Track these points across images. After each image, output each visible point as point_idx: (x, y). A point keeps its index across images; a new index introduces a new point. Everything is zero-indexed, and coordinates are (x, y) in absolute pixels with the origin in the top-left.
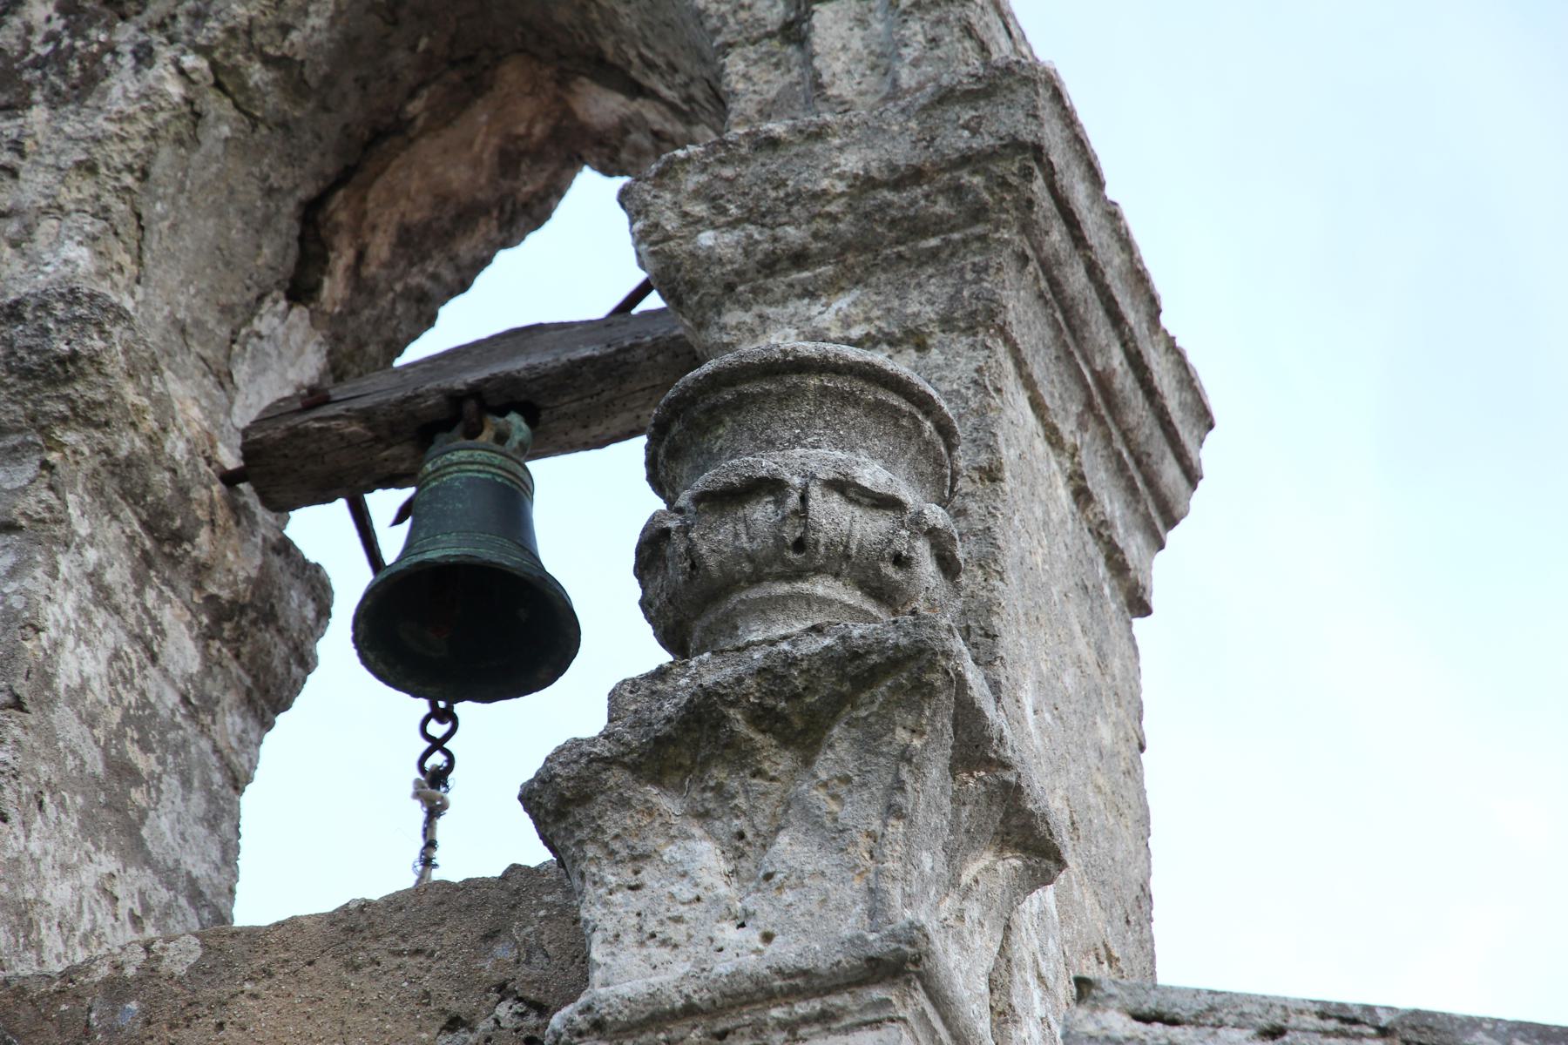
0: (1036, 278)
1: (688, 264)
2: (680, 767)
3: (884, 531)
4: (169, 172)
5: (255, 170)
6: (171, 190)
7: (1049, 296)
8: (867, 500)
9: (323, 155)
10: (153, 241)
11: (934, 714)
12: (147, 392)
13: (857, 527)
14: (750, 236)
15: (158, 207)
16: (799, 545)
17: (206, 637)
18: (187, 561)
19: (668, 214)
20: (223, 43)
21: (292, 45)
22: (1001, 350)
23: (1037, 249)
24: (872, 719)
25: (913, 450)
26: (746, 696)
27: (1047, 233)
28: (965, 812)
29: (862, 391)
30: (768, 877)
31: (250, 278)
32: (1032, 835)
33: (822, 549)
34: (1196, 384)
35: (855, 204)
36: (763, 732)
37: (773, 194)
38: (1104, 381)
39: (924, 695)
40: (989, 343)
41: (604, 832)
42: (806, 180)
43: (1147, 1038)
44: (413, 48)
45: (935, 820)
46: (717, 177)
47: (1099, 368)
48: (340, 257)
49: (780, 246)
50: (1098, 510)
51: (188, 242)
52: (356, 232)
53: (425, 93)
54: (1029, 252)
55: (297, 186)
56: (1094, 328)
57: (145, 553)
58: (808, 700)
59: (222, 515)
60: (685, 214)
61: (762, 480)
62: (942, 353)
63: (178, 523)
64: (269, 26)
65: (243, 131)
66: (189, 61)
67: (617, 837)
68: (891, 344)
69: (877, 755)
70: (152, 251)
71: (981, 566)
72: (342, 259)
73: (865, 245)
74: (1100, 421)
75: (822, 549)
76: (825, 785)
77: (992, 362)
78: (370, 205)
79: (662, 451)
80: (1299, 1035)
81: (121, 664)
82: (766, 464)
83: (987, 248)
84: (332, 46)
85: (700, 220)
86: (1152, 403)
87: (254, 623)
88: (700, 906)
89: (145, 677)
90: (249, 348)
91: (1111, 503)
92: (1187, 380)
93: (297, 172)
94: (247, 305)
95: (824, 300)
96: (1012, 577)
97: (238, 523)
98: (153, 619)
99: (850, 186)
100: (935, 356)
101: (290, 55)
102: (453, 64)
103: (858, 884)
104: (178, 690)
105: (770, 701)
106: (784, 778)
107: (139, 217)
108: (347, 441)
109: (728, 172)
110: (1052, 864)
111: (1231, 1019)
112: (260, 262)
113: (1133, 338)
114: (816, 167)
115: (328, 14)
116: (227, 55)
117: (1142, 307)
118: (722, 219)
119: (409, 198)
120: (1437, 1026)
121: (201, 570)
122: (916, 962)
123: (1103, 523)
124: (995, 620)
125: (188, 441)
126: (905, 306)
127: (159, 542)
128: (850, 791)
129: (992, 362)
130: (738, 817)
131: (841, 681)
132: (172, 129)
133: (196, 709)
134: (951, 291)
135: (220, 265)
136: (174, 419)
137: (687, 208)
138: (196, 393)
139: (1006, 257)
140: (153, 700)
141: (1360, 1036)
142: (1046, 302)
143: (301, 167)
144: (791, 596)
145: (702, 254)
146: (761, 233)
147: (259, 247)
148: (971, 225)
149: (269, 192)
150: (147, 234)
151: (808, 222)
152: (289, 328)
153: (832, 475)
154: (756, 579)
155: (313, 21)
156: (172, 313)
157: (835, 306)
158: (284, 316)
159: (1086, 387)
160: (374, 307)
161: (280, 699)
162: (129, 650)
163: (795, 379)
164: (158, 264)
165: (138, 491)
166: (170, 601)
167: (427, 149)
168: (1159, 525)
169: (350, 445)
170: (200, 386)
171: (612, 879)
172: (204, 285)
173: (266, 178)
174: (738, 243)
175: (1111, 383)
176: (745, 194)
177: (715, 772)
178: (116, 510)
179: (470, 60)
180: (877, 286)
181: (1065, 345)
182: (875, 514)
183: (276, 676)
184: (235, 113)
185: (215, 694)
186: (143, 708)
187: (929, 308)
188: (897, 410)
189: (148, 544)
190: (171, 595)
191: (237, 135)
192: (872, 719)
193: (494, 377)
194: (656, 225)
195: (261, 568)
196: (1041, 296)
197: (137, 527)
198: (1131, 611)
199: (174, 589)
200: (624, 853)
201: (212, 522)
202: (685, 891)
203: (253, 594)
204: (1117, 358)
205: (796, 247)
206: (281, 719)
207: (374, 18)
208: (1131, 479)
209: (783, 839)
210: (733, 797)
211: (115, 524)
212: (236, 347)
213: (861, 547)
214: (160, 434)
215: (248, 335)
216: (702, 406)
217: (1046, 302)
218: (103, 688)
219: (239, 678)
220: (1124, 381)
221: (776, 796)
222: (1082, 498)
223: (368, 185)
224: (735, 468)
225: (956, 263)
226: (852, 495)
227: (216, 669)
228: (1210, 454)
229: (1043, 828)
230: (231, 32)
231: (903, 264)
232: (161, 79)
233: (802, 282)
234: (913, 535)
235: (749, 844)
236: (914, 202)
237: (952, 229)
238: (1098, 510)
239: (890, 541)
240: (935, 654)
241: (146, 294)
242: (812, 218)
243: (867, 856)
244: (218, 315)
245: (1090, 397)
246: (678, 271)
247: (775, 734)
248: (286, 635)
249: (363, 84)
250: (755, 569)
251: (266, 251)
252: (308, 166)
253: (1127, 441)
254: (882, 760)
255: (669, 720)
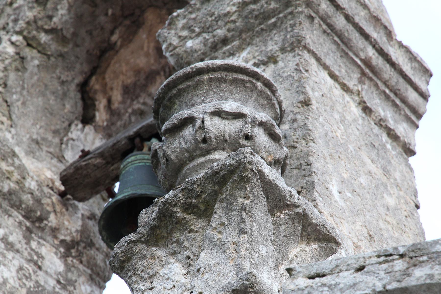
0: (320, 25)
1: (185, 56)
2: (163, 237)
3: (238, 127)
4: (15, 82)
5: (54, 75)
6: (19, 89)
7: (329, 31)
8: (230, 117)
9: (81, 64)
10: (16, 111)
11: (252, 188)
12: (13, 165)
13: (227, 128)
14: (205, 38)
15: (15, 97)
16: (204, 141)
17: (65, 257)
18: (47, 228)
19: (174, 38)
20: (26, 28)
21: (55, 23)
22: (306, 55)
23: (317, 13)
24: (228, 197)
25: (255, 95)
26: (179, 201)
27: (319, 5)
28: (282, 228)
29: (226, 76)
30: (199, 270)
31: (63, 117)
32: (320, 234)
33: (214, 140)
34: (419, 59)
35: (241, 14)
36: (190, 214)
37: (210, 19)
38: (367, 62)
39: (245, 182)
40: (300, 53)
41: (138, 270)
42: (222, 10)
43: (313, 285)
44: (106, 14)
45: (264, 232)
46: (190, 19)
47: (363, 58)
48: (100, 102)
49: (216, 38)
50: (377, 115)
51: (31, 108)
52: (105, 92)
53: (117, 31)
54: (313, 14)
55: (74, 79)
56: (355, 41)
57: (28, 228)
58: (204, 196)
59: (58, 208)
60: (180, 37)
61: (186, 119)
62: (283, 62)
63: (39, 213)
64: (43, 18)
65: (44, 61)
66: (14, 38)
67: (143, 271)
68: (264, 64)
69: (233, 211)
70: (16, 114)
71: (304, 139)
72: (101, 104)
73: (248, 29)
74: (371, 79)
75: (214, 140)
76: (215, 228)
77: (302, 60)
78: (107, 80)
79: (159, 122)
80: (370, 266)
81: (23, 272)
82: (186, 113)
83: (294, 16)
84: (72, 20)
85: (185, 38)
86: (395, 69)
87: (85, 248)
88: (175, 289)
89: (37, 276)
90: (69, 145)
91: (384, 111)
92: (413, 58)
93: (72, 73)
94: (65, 129)
95: (237, 55)
96: (320, 141)
97: (67, 210)
98: (37, 254)
99: (238, 7)
100: (281, 64)
101: (55, 27)
102: (126, 17)
103: (232, 263)
104: (55, 279)
105: (189, 201)
106: (201, 230)
107: (6, 102)
108: (97, 167)
109: (193, 16)
110: (333, 245)
111: (344, 268)
112: (66, 111)
113: (377, 43)
114: (224, 4)
115: (66, 8)
116: (29, 33)
117: (381, 31)
118: (194, 35)
119: (123, 74)
120: (422, 248)
121: (54, 231)
122: (252, 287)
123: (381, 120)
124: (311, 158)
125: (37, 181)
126: (267, 48)
127: (33, 222)
128: (225, 228)
129: (302, 60)
130: (186, 250)
131: (214, 185)
132: (13, 66)
133: (64, 285)
134: (282, 37)
135: (48, 115)
136: (28, 174)
137: (181, 34)
138: (49, 166)
139: (302, 18)
140: (42, 283)
141: (393, 260)
142: (328, 34)
143: (73, 71)
144: (206, 162)
145: (189, 50)
146: (208, 35)
147: (64, 105)
148: (286, 9)
149: (63, 83)
150: (12, 108)
151: (225, 26)
152: (86, 135)
153: (213, 110)
154: (192, 159)
155: (61, 12)
156: (31, 137)
157: (242, 56)
158: (82, 130)
159: (359, 66)
160: (122, 120)
161: (105, 276)
162: (27, 266)
163: (198, 78)
164: (19, 118)
165: (18, 203)
166: (44, 245)
167: (125, 53)
168: (413, 118)
169: (98, 168)
170: (50, 163)
171: (142, 288)
172: (43, 124)
173: (59, 78)
174: (201, 42)
175: (371, 63)
176: (200, 22)
177: (175, 235)
178: (10, 213)
179: (132, 14)
180: (256, 44)
181: (343, 50)
182: (234, 121)
183: (100, 267)
184: (39, 55)
185: (74, 279)
186: (38, 287)
187: (275, 46)
188: (243, 80)
189: (28, 224)
190: (44, 243)
191: (42, 63)
192: (228, 197)
193: (143, 127)
194: (170, 44)
195: (82, 226)
196: (325, 32)
197: (21, 218)
198: (407, 155)
199: (45, 240)
200: (146, 276)
201: (55, 211)
202: (169, 285)
203: (81, 236)
204: (371, 52)
205: (223, 37)
206: (108, 284)
207: (86, 6)
208: (393, 101)
209: (203, 254)
210: (183, 243)
211: (11, 219)
212: (64, 146)
213: (230, 136)
214: (22, 180)
215: (68, 140)
216: (167, 99)
217: (328, 34)
218: (15, 281)
219: (84, 271)
220: (377, 61)
221: (199, 238)
222: (367, 111)
223: (104, 72)
224: (175, 117)
225: (284, 26)
226: (224, 116)
227: (73, 269)
228: (433, 87)
229: (324, 230)
230: (28, 23)
231: (264, 32)
232: (5, 48)
233: (228, 50)
234: (253, 127)
235: (192, 260)
236: (262, 6)
237: (280, 13)
238: (377, 115)
239: (242, 130)
240: (245, 164)
241: (17, 131)
242: (226, 24)
243: (234, 252)
244: (52, 135)
245: (362, 70)
246: (182, 59)
247: (195, 214)
248: (101, 250)
249: (90, 33)
250: (190, 155)
251: (68, 106)
252: (76, 70)
253: (387, 86)
254: (235, 213)
255: (154, 219)
